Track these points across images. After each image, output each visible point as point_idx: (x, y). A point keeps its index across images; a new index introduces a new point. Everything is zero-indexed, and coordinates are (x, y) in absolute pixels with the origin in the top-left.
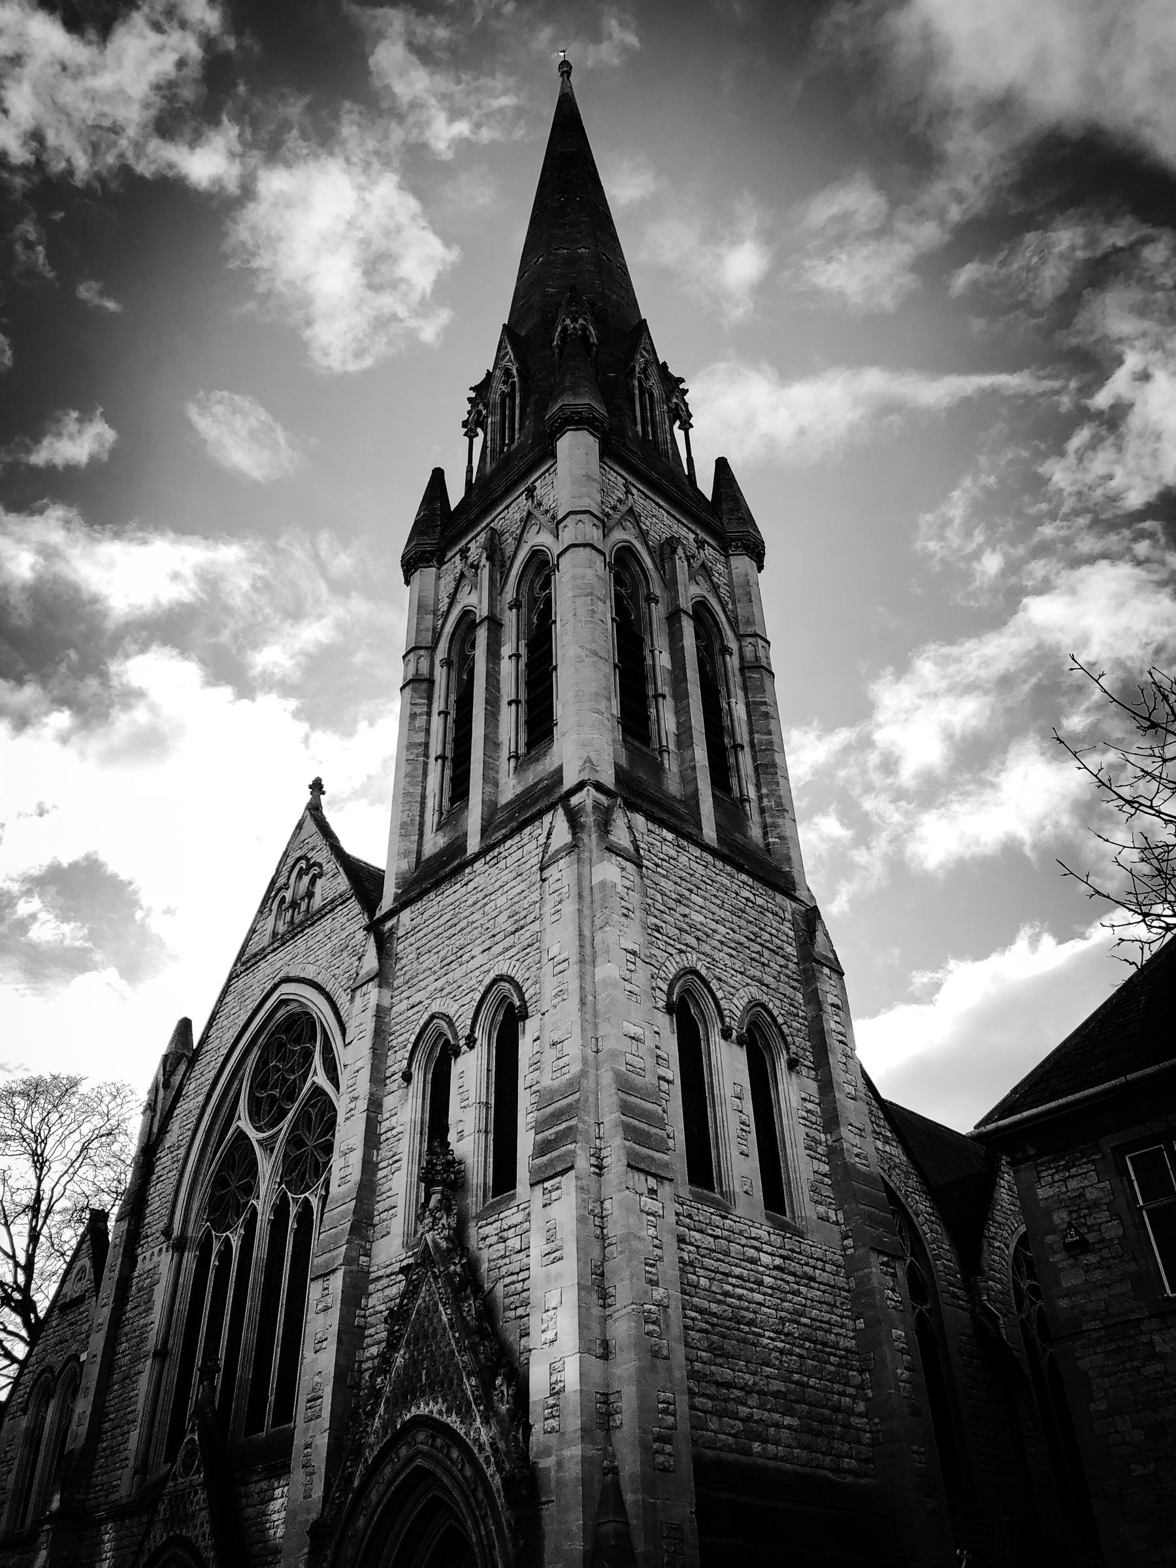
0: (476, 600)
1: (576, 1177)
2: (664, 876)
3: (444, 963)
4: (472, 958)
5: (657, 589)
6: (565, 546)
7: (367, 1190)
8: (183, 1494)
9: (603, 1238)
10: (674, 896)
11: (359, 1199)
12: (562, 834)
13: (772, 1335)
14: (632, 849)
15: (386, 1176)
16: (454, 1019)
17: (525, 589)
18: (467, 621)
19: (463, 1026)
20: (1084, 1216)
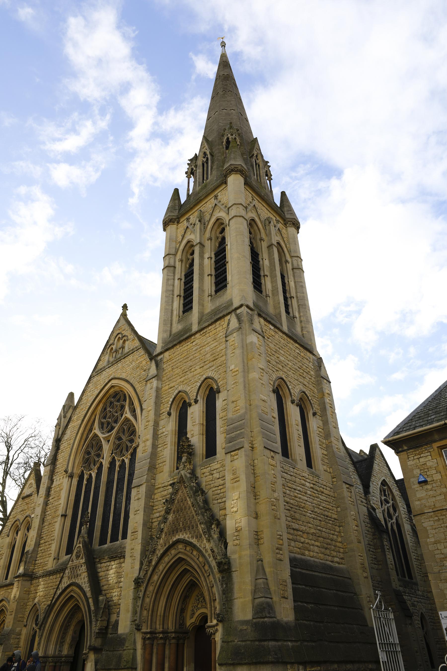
0: (194, 237)
1: (245, 451)
2: (270, 342)
3: (183, 372)
4: (196, 370)
5: (263, 236)
6: (232, 216)
7: (154, 455)
8: (76, 567)
9: (254, 474)
10: (274, 350)
11: (151, 458)
12: (234, 323)
13: (311, 512)
14: (261, 331)
15: (161, 450)
16: (189, 393)
17: (213, 232)
18: (190, 246)
19: (193, 395)
20: (426, 472)
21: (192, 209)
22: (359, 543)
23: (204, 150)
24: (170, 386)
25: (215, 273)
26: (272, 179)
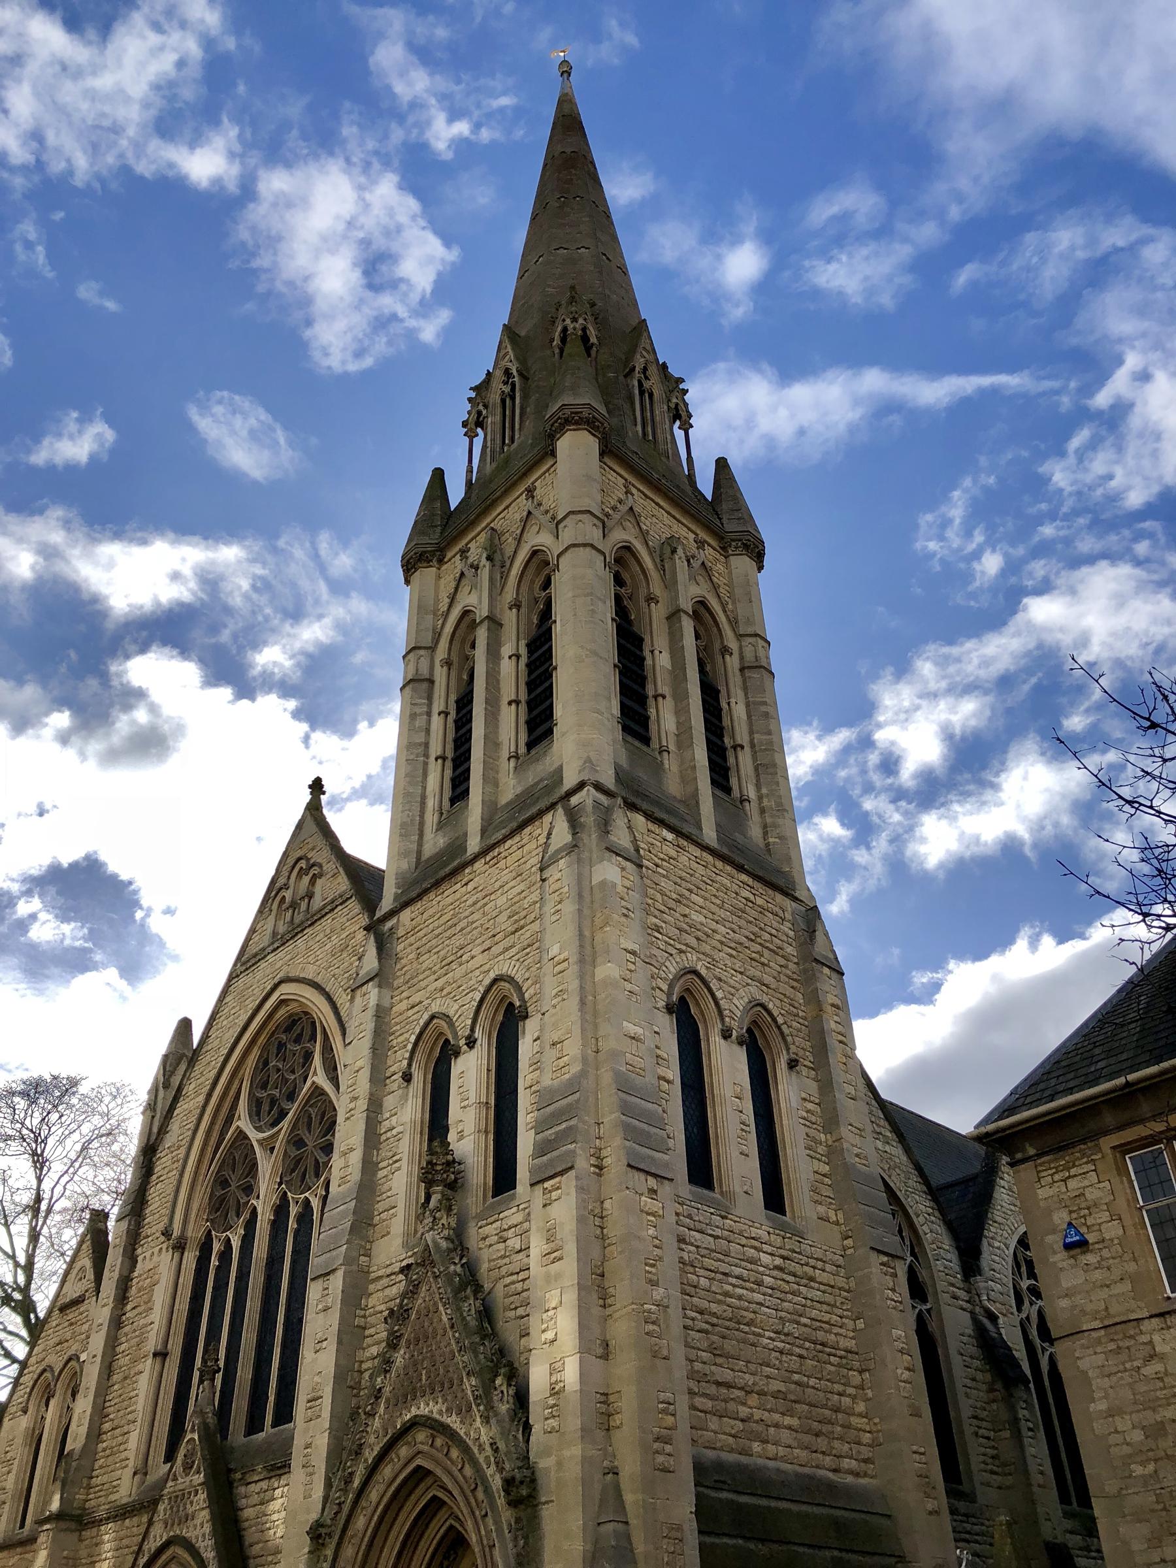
0: (476, 600)
2: (664, 876)
5: (657, 588)
9: (603, 1238)
10: (674, 896)
12: (562, 833)
13: (772, 1335)
14: (632, 849)
17: (524, 588)
19: (463, 1025)
20: (1084, 1217)
21: (473, 524)
22: (916, 1415)
23: (505, 363)
24: (413, 1000)
25: (529, 695)
26: (692, 426)
